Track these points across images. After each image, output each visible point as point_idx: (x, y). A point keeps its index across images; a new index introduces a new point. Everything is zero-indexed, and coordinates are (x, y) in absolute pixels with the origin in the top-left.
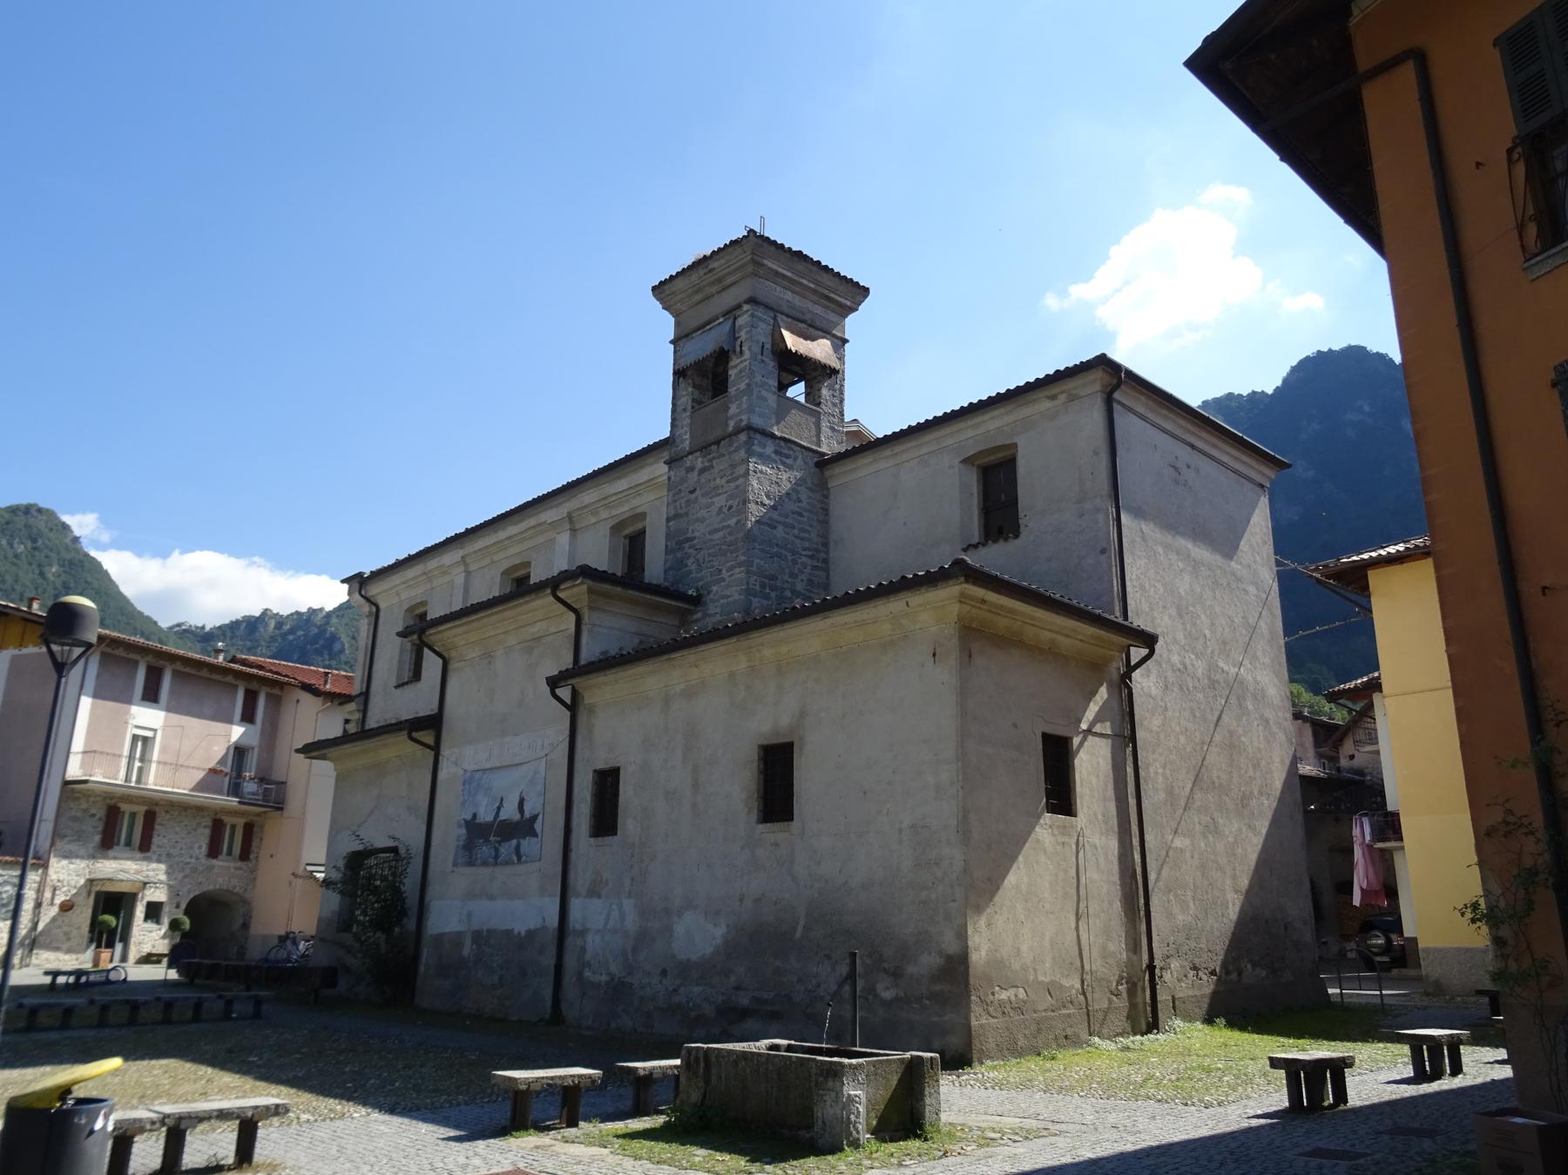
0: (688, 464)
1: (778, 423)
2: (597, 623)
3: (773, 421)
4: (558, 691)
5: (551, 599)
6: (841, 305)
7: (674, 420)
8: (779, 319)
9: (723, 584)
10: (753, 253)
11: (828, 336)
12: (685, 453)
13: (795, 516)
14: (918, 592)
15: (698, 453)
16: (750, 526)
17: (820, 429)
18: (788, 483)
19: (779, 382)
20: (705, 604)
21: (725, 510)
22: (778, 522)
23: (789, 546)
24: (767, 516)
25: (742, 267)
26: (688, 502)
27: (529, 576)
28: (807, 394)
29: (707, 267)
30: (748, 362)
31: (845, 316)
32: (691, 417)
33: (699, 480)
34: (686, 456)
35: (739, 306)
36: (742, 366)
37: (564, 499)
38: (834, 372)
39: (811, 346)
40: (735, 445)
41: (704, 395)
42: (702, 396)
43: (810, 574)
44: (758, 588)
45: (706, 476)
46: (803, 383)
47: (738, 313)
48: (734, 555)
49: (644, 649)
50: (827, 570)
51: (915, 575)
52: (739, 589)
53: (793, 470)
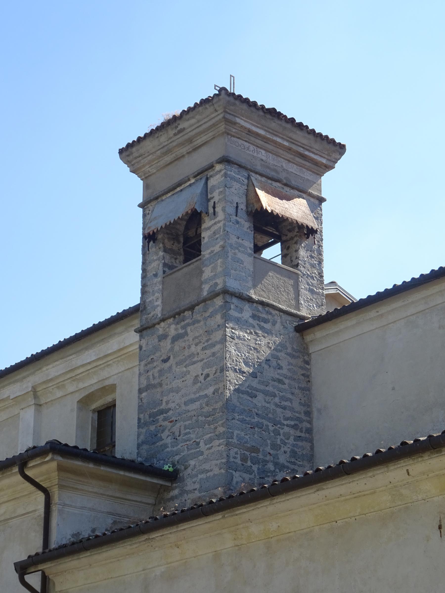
0: (161, 332)
1: (255, 286)
2: (67, 502)
3: (250, 284)
4: (28, 578)
5: (19, 478)
6: (316, 163)
7: (144, 286)
8: (252, 178)
9: (201, 458)
10: (225, 112)
11: (304, 196)
12: (157, 320)
13: (276, 384)
14: (420, 459)
15: (171, 320)
16: (228, 395)
17: (299, 291)
18: (267, 349)
19: (255, 246)
20: (182, 480)
21: (201, 378)
22: (257, 390)
23: (270, 415)
24: (247, 385)
25: (214, 125)
26: (161, 372)
27: (115, 406)
28: (284, 256)
29: (176, 127)
30: (222, 222)
31: (321, 175)
32: (163, 283)
33: (172, 349)
34: (159, 324)
35: (211, 167)
36: (216, 227)
37: (27, 373)
38: (311, 232)
39: (287, 206)
40: (211, 310)
41: (176, 259)
42: (173, 260)
43: (294, 445)
44: (239, 461)
45: (180, 343)
46: (279, 244)
47: (210, 173)
48: (212, 426)
49: (121, 529)
50: (311, 441)
51: (416, 441)
52: (218, 462)
53: (272, 334)
